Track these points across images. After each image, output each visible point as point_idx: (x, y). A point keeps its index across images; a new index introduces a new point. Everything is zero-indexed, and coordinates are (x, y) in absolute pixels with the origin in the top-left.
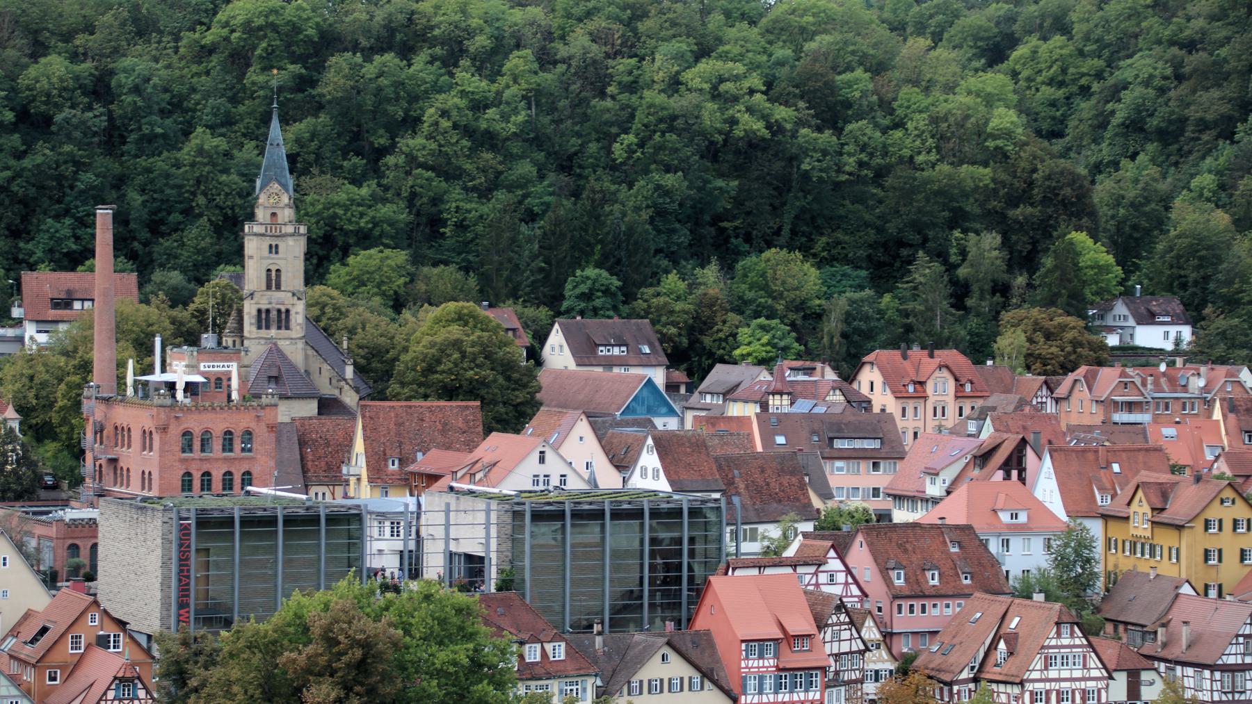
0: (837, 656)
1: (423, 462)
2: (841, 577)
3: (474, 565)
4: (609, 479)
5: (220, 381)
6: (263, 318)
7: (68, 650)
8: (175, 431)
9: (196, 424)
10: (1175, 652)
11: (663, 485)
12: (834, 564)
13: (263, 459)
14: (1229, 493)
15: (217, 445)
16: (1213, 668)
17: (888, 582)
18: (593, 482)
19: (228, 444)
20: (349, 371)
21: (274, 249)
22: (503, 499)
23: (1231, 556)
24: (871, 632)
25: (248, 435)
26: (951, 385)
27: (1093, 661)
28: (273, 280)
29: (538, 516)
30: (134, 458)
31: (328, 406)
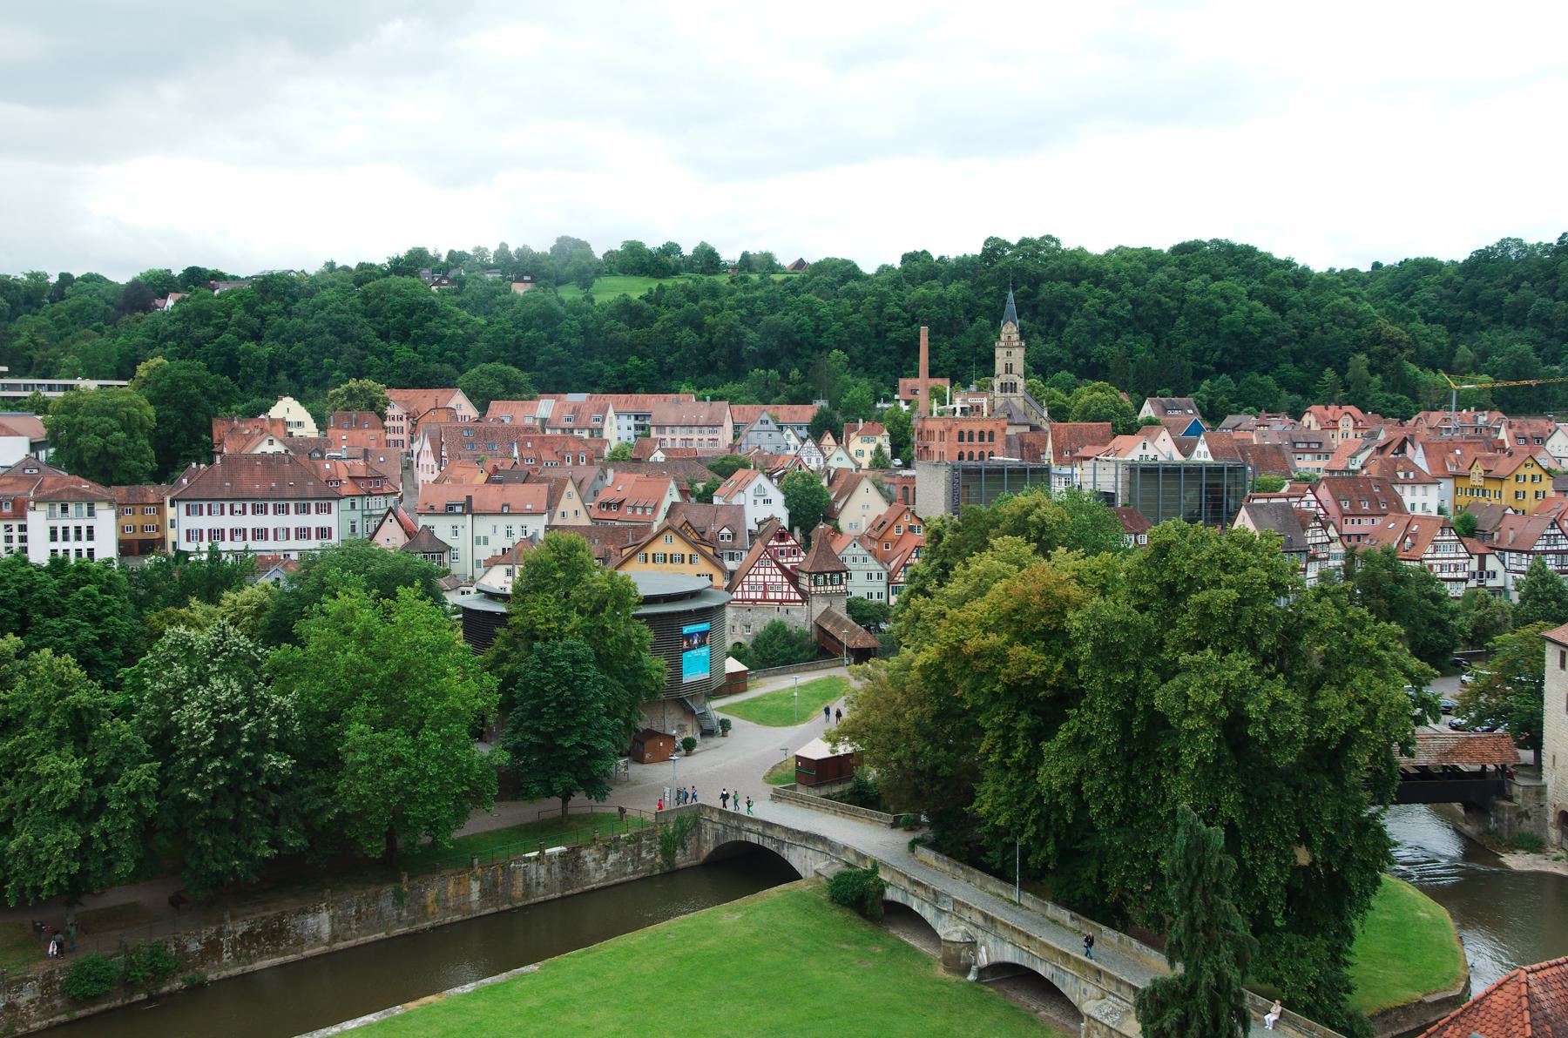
0: (1315, 545)
1: (1082, 452)
2: (1314, 504)
3: (1109, 498)
4: (1178, 458)
5: (978, 408)
6: (1004, 388)
7: (894, 533)
8: (955, 431)
9: (966, 427)
10: (1505, 546)
11: (1210, 459)
12: (1311, 497)
13: (999, 444)
14: (1530, 461)
15: (976, 438)
16: (1528, 553)
17: (1340, 507)
18: (1171, 458)
19: (981, 438)
20: (1045, 414)
21: (1009, 354)
22: (1124, 463)
23: (1530, 495)
24: (1332, 532)
25: (991, 434)
26: (1351, 423)
27: (1461, 549)
28: (1009, 369)
29: (1144, 470)
30: (935, 445)
31: (1034, 428)
